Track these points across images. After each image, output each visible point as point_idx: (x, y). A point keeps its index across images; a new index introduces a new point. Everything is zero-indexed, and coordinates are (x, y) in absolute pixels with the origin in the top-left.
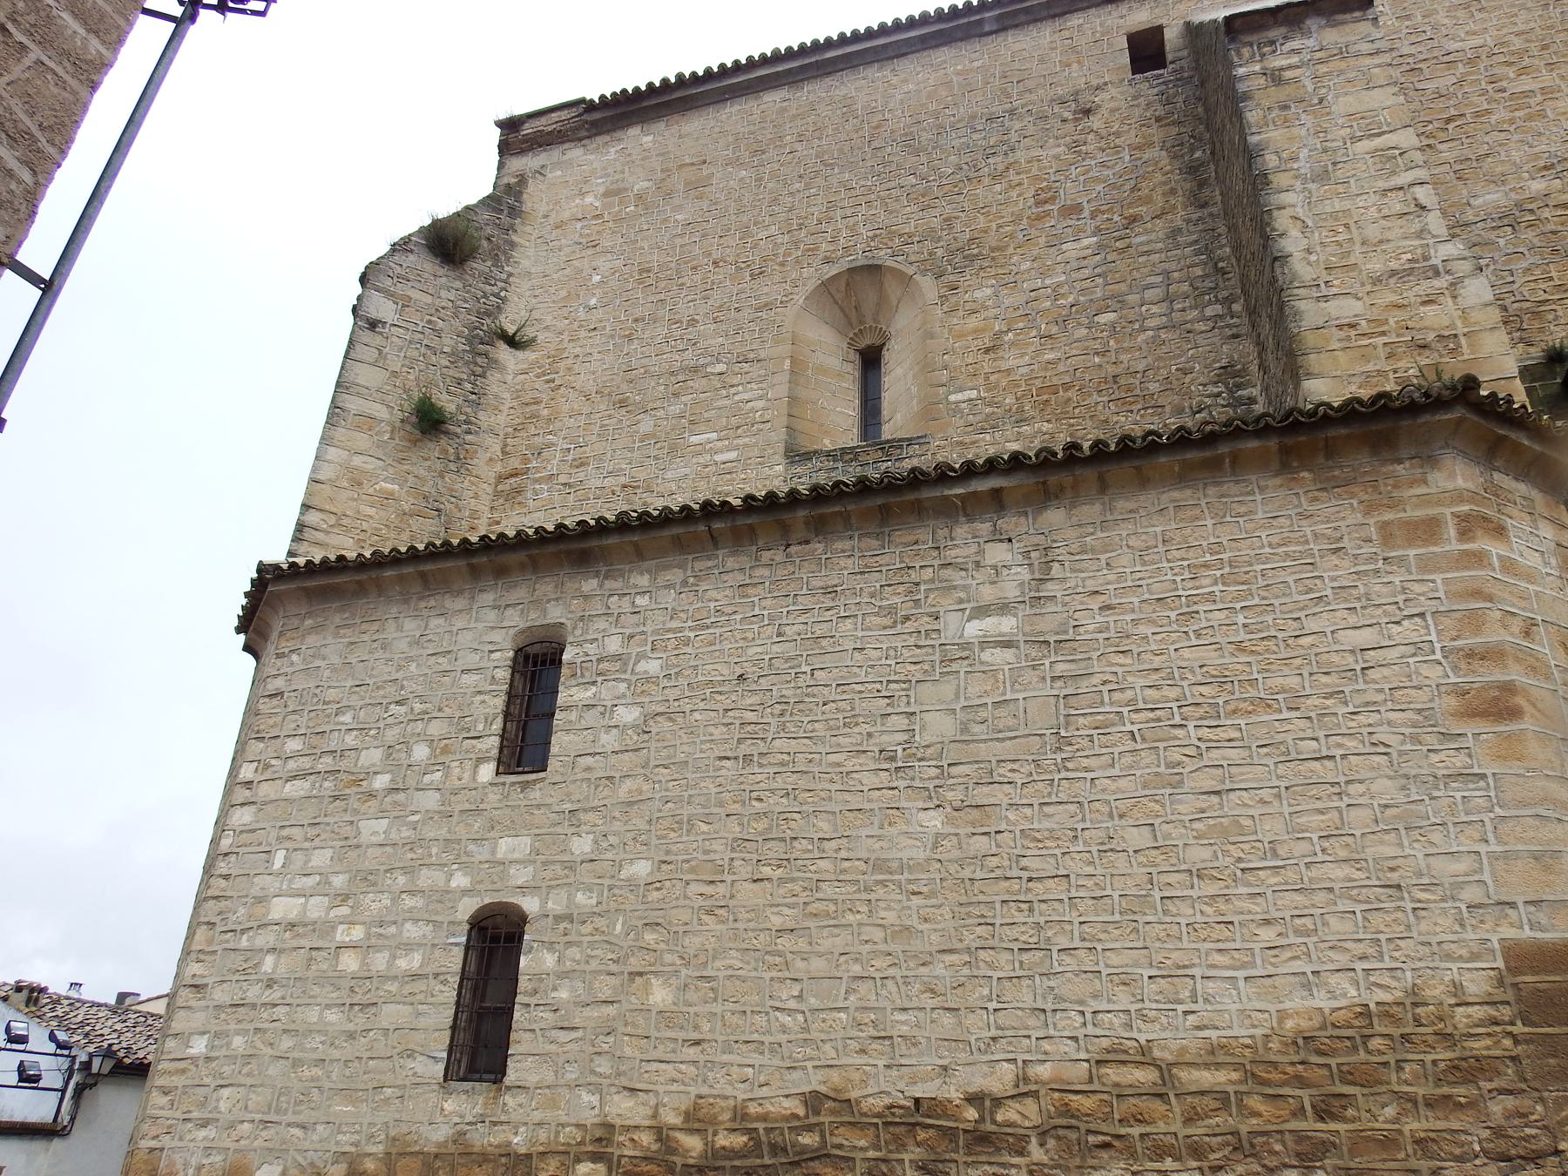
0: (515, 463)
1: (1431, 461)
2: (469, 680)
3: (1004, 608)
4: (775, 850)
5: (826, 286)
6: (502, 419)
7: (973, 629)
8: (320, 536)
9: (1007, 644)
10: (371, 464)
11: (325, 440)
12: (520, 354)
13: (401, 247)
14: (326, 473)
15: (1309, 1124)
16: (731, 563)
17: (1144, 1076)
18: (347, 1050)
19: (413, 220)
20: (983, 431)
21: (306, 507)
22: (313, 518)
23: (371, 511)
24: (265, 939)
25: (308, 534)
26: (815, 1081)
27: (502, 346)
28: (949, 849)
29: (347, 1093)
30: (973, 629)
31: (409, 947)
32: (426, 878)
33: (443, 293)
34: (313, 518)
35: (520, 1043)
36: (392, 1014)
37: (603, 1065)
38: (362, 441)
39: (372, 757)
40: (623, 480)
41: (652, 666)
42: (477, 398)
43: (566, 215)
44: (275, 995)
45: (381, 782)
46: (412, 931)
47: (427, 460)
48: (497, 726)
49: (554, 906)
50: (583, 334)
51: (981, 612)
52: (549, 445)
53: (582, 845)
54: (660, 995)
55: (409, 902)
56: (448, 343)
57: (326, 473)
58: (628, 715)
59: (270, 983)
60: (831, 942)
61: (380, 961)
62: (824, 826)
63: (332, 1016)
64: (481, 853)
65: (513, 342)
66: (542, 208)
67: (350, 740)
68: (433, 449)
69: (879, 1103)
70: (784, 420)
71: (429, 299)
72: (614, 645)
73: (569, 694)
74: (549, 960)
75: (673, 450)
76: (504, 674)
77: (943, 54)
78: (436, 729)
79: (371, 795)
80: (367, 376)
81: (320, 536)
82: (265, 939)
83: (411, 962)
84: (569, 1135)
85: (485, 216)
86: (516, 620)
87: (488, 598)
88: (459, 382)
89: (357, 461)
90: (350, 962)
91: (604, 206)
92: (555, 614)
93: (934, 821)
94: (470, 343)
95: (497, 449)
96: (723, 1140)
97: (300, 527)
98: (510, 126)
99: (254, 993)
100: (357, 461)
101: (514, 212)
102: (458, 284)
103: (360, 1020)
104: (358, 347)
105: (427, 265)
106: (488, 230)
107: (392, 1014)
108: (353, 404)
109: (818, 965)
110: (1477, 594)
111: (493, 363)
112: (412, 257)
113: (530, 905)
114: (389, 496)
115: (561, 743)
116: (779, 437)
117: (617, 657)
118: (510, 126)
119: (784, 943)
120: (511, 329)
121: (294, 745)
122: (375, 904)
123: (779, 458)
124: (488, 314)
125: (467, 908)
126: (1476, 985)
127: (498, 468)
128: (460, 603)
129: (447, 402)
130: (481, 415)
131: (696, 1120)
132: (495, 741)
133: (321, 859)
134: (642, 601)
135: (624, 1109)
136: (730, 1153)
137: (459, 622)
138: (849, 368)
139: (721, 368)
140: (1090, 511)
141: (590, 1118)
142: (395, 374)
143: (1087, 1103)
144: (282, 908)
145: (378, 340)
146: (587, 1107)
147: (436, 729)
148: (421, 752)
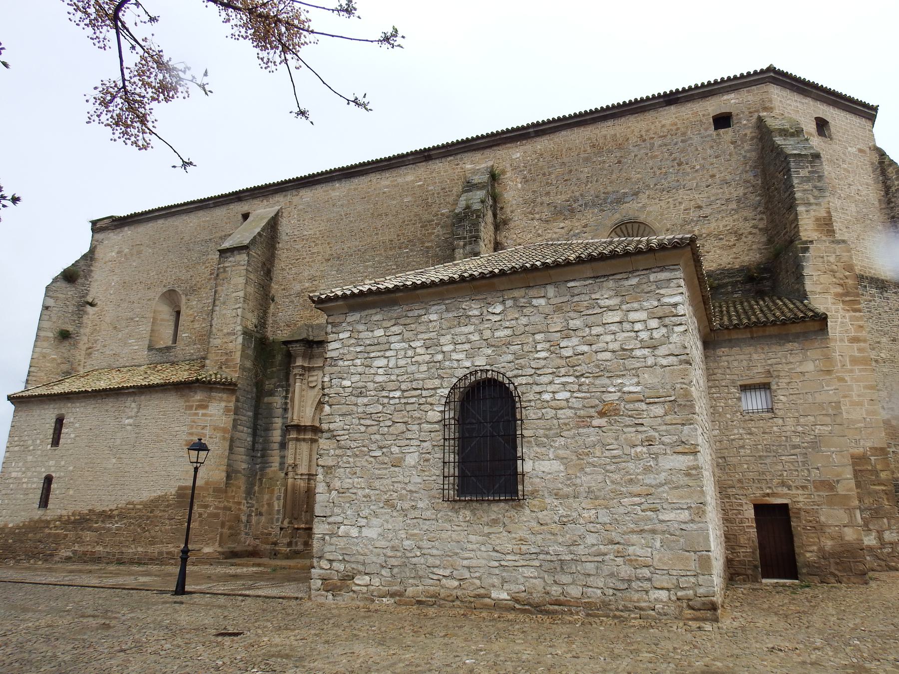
0: (90, 345)
1: (196, 393)
2: (48, 425)
3: (131, 417)
4: (91, 465)
5: (164, 294)
6: (88, 330)
7: (127, 421)
8: (35, 374)
9: (131, 425)
10: (48, 351)
11: (35, 346)
12: (94, 308)
13: (55, 280)
14: (36, 356)
15: (149, 514)
16: (93, 402)
17: (131, 506)
18: (24, 503)
19: (58, 271)
20: (187, 346)
21: (30, 366)
22: (33, 369)
23: (49, 365)
24: (11, 481)
25: (31, 374)
26: (90, 507)
27: (88, 306)
28: (116, 466)
29: (24, 510)
30: (127, 421)
31: (34, 483)
32: (38, 469)
33: (69, 293)
34: (33, 369)
35: (50, 501)
36: (31, 496)
37: (62, 505)
38: (45, 344)
39: (30, 442)
40: (114, 352)
41: (77, 425)
42: (80, 325)
43: (107, 259)
44: (12, 492)
45: (31, 448)
46: (35, 480)
47: (64, 348)
48: (52, 437)
49: (58, 475)
50: (109, 303)
51: (128, 418)
52: (98, 340)
53: (63, 463)
54: (71, 492)
55: (35, 474)
56: (71, 309)
57: (36, 356)
58: (72, 436)
59: (12, 490)
60: (96, 483)
61: (29, 485)
62: (99, 461)
63: (22, 496)
64: (47, 464)
65: (92, 305)
66: (101, 256)
67: (27, 438)
68: (66, 343)
69: (98, 511)
70: (148, 338)
71: (64, 296)
72: (72, 420)
73: (64, 430)
74: (56, 485)
75: (125, 344)
76: (53, 425)
77: (201, 213)
78: (41, 437)
79: (29, 451)
80: (46, 324)
81: (35, 374)
82: (11, 481)
83: (34, 486)
84: (56, 517)
85: (82, 263)
86: (56, 412)
87: (52, 406)
88: (74, 321)
89: (44, 351)
90: (25, 486)
91: (117, 257)
92: (63, 411)
93: (114, 461)
94: (77, 307)
95: (86, 340)
96: (77, 517)
97: (29, 372)
98: (94, 223)
99: (9, 492)
100: (44, 351)
101: (92, 259)
102: (74, 289)
103: (26, 497)
104: (43, 316)
105: (63, 284)
106: (83, 268)
107: (31, 496)
108: (42, 334)
109: (94, 487)
110: (194, 422)
111: (86, 313)
112: (58, 283)
113: (54, 475)
114: (54, 359)
115: (61, 441)
116: (147, 342)
117: (72, 423)
118: (94, 223)
119: (90, 483)
120: (90, 301)
121: (16, 439)
122: (29, 474)
123: (146, 349)
124: (83, 297)
125: (44, 475)
126: (173, 493)
127: (87, 346)
128: (47, 407)
129: (70, 328)
130: (82, 330)
131: (73, 514)
132: (51, 440)
133: (20, 464)
134: (78, 410)
135: (64, 513)
136: (78, 520)
137: (47, 412)
138: (172, 317)
139: (137, 319)
140: (148, 397)
141: (59, 514)
142: (54, 322)
143: (123, 511)
144: (14, 475)
145: (49, 313)
146: (59, 512)
147: (41, 437)
148: (38, 442)
